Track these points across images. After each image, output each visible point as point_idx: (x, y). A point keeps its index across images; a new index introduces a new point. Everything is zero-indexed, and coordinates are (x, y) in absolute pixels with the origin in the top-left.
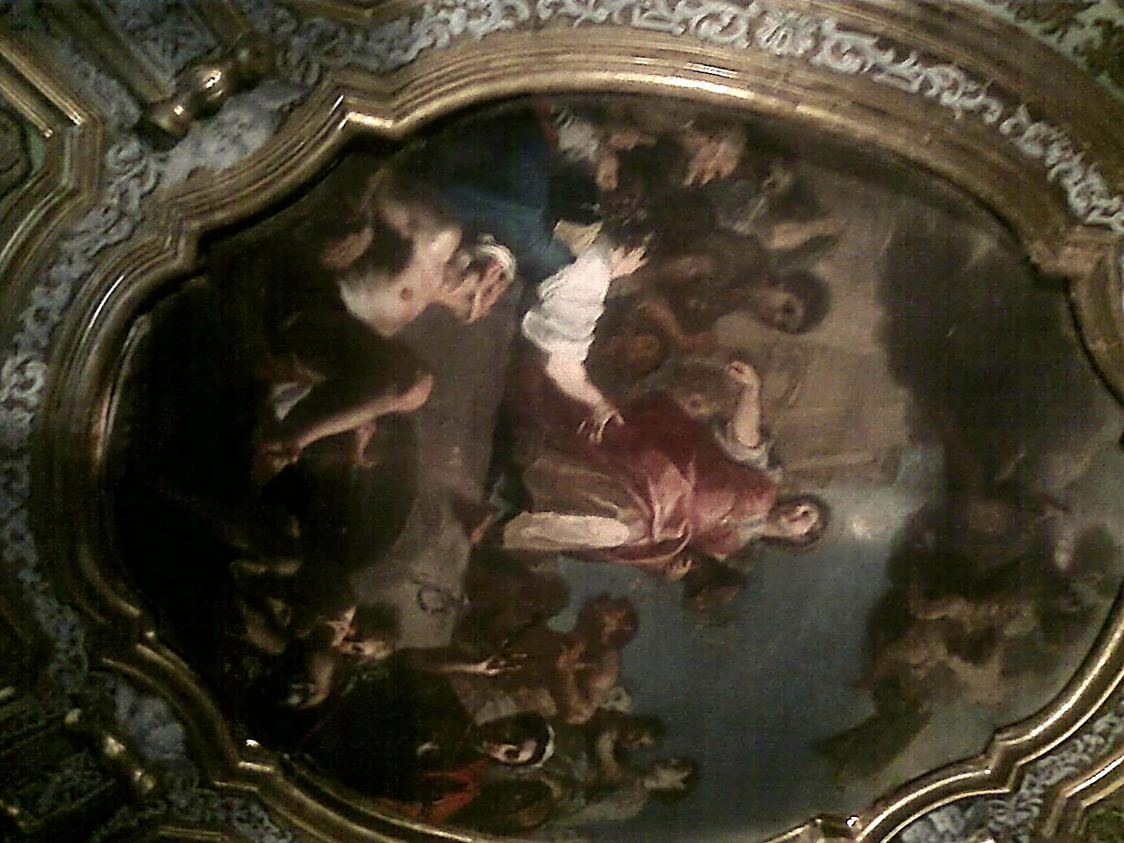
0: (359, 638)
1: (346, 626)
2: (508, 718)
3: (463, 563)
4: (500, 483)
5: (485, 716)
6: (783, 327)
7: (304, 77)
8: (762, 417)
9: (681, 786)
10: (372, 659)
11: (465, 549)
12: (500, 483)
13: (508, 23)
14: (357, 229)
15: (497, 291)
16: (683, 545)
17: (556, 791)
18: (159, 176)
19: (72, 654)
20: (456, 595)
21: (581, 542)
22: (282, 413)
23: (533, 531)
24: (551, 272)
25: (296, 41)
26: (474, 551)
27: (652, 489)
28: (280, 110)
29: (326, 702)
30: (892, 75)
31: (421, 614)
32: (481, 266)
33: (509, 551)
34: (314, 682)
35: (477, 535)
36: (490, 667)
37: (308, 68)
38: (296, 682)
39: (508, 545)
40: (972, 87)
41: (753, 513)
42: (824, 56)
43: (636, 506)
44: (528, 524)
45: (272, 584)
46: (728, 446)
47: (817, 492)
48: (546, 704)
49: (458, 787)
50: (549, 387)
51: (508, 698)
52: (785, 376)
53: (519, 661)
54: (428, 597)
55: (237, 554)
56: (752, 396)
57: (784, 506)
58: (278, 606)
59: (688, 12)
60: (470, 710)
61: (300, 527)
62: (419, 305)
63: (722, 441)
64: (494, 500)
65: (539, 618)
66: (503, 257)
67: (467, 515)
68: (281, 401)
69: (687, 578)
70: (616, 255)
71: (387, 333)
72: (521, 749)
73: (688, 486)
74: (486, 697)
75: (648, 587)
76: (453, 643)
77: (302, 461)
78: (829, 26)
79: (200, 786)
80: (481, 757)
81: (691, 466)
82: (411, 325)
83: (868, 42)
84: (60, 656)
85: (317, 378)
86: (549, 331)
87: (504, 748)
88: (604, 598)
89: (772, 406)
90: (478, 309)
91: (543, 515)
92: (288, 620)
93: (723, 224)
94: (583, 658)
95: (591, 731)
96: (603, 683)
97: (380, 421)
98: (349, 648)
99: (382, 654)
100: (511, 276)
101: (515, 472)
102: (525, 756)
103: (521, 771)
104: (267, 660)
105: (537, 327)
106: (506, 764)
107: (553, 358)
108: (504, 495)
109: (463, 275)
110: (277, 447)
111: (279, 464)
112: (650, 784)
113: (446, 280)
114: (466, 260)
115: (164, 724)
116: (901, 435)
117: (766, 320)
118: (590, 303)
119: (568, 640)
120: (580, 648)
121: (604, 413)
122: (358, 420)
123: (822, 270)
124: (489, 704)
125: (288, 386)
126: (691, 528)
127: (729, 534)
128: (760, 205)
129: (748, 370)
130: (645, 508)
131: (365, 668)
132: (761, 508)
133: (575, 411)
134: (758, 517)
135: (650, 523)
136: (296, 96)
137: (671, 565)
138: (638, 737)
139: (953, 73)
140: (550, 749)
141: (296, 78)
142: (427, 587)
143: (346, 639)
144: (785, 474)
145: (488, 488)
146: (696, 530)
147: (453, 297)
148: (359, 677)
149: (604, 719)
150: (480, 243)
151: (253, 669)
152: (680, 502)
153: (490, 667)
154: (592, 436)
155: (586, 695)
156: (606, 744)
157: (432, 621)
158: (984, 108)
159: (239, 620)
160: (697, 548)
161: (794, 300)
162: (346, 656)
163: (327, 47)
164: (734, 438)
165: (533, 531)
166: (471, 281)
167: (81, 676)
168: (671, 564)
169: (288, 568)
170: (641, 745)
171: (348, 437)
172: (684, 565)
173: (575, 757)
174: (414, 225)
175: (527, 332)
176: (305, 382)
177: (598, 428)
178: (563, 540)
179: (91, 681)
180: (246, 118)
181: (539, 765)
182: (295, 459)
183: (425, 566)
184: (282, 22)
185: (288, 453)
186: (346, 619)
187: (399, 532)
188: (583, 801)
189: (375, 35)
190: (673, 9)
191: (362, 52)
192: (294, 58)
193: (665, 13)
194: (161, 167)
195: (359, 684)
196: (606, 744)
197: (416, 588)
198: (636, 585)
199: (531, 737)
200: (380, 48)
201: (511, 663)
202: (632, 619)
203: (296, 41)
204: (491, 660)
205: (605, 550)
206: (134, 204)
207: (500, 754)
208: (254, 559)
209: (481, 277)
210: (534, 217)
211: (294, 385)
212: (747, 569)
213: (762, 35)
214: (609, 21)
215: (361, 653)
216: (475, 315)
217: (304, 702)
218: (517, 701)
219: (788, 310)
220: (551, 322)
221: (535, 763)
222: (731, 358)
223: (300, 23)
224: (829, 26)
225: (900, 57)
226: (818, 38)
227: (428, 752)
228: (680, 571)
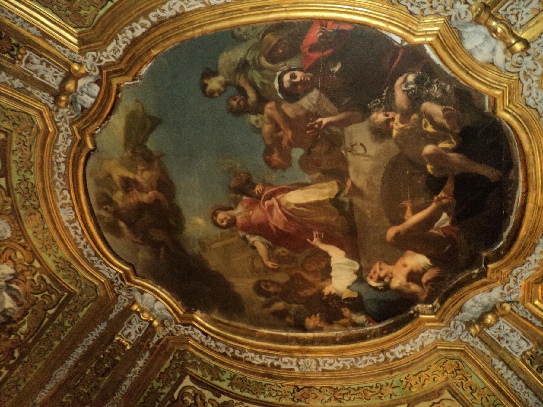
0: (388, 122)
1: (395, 126)
2: (303, 97)
3: (351, 169)
4: (347, 208)
5: (315, 93)
6: (266, 281)
7: (455, 323)
8: (257, 252)
9: (206, 81)
10: (378, 112)
11: (353, 177)
12: (347, 208)
13: (392, 350)
14: (428, 282)
15: (372, 273)
16: (262, 199)
17: (263, 60)
18: (503, 289)
19: (529, 80)
20: (349, 154)
21: (304, 191)
22: (445, 216)
23: (326, 191)
24: (354, 282)
25: (460, 333)
26: (348, 177)
27: (285, 218)
28: (462, 312)
29: (394, 81)
30: (272, 359)
31: (362, 141)
32: (380, 279)
33: (333, 180)
34: (404, 91)
35: (349, 183)
36: (321, 122)
37: (454, 327)
38: (413, 89)
39: (334, 182)
40: (248, 359)
41: (241, 218)
42: (294, 360)
43: (288, 210)
44: (330, 193)
45: (435, 140)
46: (265, 240)
47: (223, 231)
48: (289, 109)
49: (313, 48)
50: (341, 246)
51: (308, 108)
52: (257, 267)
53: (309, 129)
54: (361, 150)
55: (454, 150)
56: (265, 259)
57: (232, 223)
58: (430, 129)
59: (339, 364)
60: (322, 95)
61: (427, 169)
62: (399, 263)
63: (267, 241)
64: (347, 200)
65: (309, 152)
66: (373, 283)
67: (356, 190)
68: (445, 220)
69: (254, 186)
70: (333, 291)
71: (409, 252)
72: (290, 81)
73: (272, 223)
74: (317, 105)
75: (268, 179)
76: (342, 130)
77: (432, 198)
78: (297, 369)
79: (450, 17)
80: (308, 71)
81: (274, 230)
82: (402, 255)
83: (283, 366)
84: (535, 79)
85: (433, 231)
86: (348, 264)
87: (298, 79)
88: (284, 168)
89: (256, 256)
90: (377, 267)
91: (325, 198)
92: (423, 123)
93: (302, 306)
94: (280, 139)
95: (262, 100)
96: (267, 128)
97: (404, 221)
98: (391, 114)
99: (374, 115)
100: (368, 279)
101: (342, 213)
102: (287, 78)
103: (286, 68)
104: (429, 98)
105: (354, 265)
106: (294, 69)
107: (343, 256)
108: (344, 203)
109: (386, 276)
110: (444, 201)
111: (442, 194)
112: (221, 78)
113: (391, 273)
114: (386, 280)
115: (476, 47)
116: (205, 256)
117: (273, 283)
118: (337, 276)
119: (291, 145)
120: (285, 143)
121: (316, 242)
122: (412, 219)
123: (262, 299)
124: (314, 102)
125: (445, 225)
126: (262, 206)
127: (247, 208)
128: (292, 312)
129: (271, 266)
130: (284, 210)
131: (380, 106)
132: (240, 220)
133: (328, 240)
134: (240, 217)
135: (280, 205)
136: (457, 317)
137: (263, 189)
138: (238, 103)
139: (255, 362)
140: (276, 85)
141: (458, 322)
142: (364, 155)
143: (393, 119)
144: (238, 235)
145: (351, 204)
146: (260, 207)
147: (387, 268)
148: (381, 100)
149: (258, 109)
150: (382, 286)
151: (435, 91)
152: (272, 215)
153: (321, 122)
154: (317, 233)
155: (272, 120)
156: (252, 96)
157: (354, 140)
158: (241, 354)
159: (447, 117)
160: (256, 200)
161: (266, 289)
162: (391, 110)
163: (449, 333)
164: (263, 243)
165: (326, 191)
166: (382, 274)
167: (524, 68)
168: (263, 190)
169: (429, 149)
170: (235, 100)
171: (415, 211)
172: (258, 191)
173: (262, 83)
174: (408, 287)
175: (356, 263)
176: (437, 229)
177: (316, 236)
178: (312, 190)
179: (519, 65)
180: (474, 309)
181: (278, 74)
182: (436, 198)
183: (366, 164)
184: (465, 337)
185: (439, 200)
186: (396, 130)
187: (383, 178)
188: (248, 58)
189: (434, 339)
190: (343, 364)
191: (437, 333)
192: (460, 328)
193: (345, 363)
194: (502, 291)
195: (380, 96)
196: (252, 96)
197: (368, 153)
198: (272, 177)
199: (289, 88)
200: (431, 335)
201: (312, 127)
202: (269, 163)
203: (460, 333)
204: (322, 126)
205: (293, 190)
206: (512, 279)
207: (299, 75)
208: (446, 149)
209: (379, 276)
210: (366, 297)
211: (441, 226)
212: (232, 195)
213: (314, 363)
214: (361, 357)
215: (384, 113)
216: (378, 264)
217: (406, 79)
218: (302, 108)
219: (267, 286)
220: (348, 268)
221: (281, 74)
222: (279, 268)
223: (459, 339)
224: (297, 369)
225: (272, 365)
226: (298, 365)
227: (335, 66)
228: (258, 188)
